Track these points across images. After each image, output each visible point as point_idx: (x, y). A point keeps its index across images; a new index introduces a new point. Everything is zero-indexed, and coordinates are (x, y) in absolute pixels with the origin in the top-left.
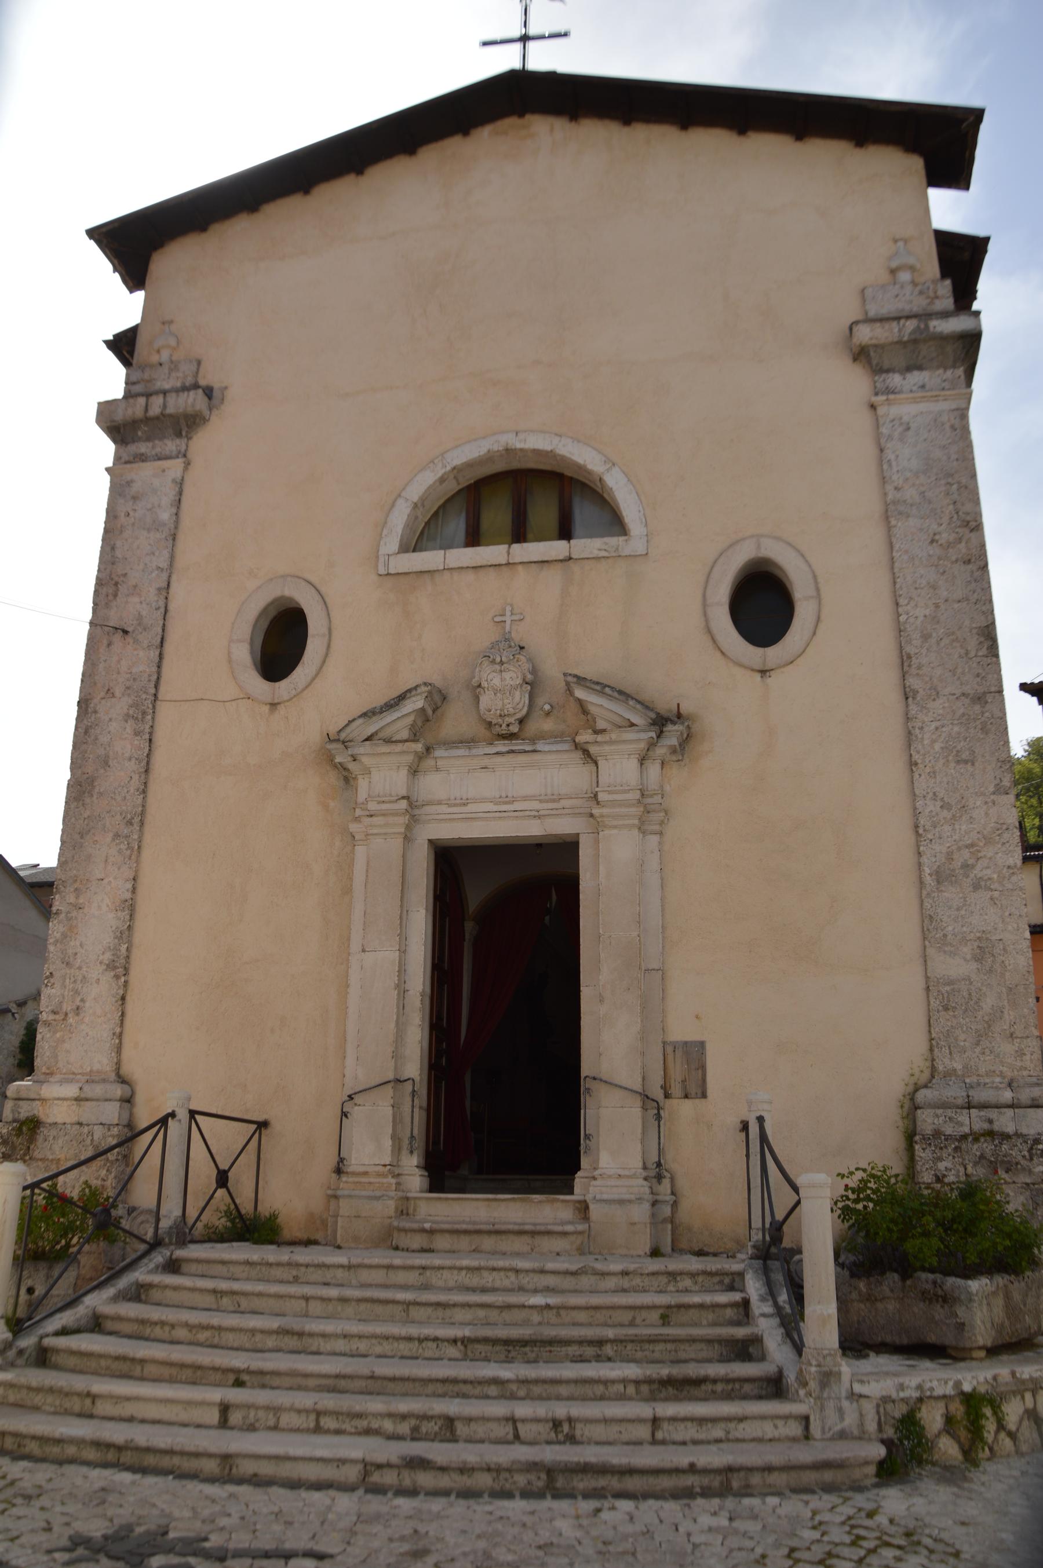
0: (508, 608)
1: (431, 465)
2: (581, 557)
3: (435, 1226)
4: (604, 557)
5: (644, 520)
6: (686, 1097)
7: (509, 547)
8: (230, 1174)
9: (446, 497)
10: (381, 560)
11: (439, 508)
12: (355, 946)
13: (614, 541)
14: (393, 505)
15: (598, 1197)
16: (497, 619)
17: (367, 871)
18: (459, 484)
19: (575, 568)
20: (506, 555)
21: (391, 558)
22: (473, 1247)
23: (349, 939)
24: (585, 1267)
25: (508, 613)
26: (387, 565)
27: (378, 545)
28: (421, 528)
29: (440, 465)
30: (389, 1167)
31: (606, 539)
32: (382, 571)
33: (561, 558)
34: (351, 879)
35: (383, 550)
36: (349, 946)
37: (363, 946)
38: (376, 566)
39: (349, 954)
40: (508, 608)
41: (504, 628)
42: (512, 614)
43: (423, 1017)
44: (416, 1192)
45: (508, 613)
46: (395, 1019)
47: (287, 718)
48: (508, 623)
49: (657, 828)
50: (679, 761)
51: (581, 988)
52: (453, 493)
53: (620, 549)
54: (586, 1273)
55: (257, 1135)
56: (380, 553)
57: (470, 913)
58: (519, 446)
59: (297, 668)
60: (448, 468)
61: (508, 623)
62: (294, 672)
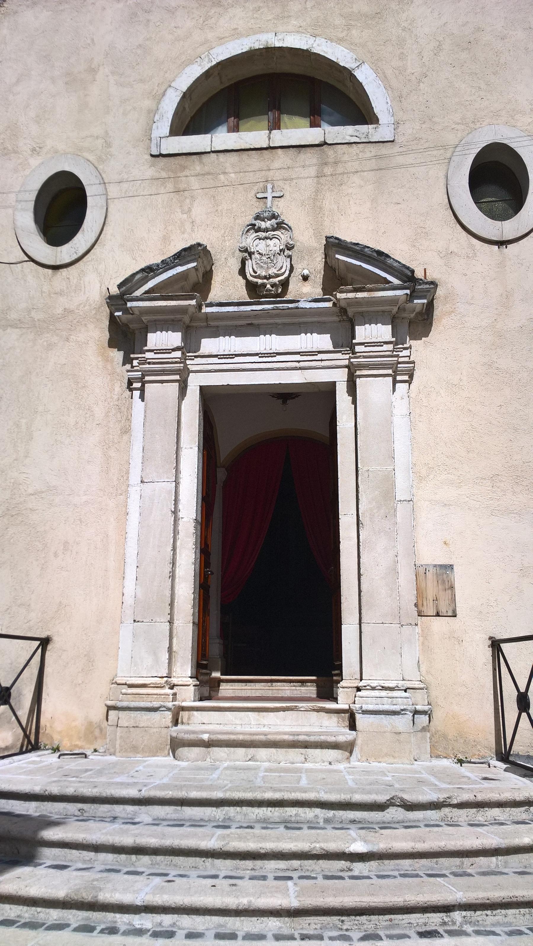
0: (269, 186)
1: (199, 60)
2: (335, 142)
3: (214, 737)
4: (355, 143)
5: (391, 111)
6: (438, 615)
7: (270, 133)
8: (12, 691)
9: (209, 95)
10: (154, 142)
11: (204, 104)
12: (135, 477)
13: (363, 128)
14: (164, 94)
15: (365, 707)
16: (259, 196)
17: (145, 412)
18: (221, 83)
19: (329, 151)
20: (267, 139)
21: (162, 140)
22: (250, 757)
23: (128, 473)
24: (392, 798)
25: (269, 190)
26: (159, 146)
27: (151, 129)
28: (187, 123)
29: (207, 59)
30: (165, 679)
31: (357, 127)
32: (155, 152)
33: (317, 143)
34: (129, 420)
35: (155, 134)
36: (128, 479)
37: (142, 477)
38: (149, 148)
39: (128, 486)
40: (269, 186)
41: (265, 203)
42: (273, 191)
43: (196, 541)
44: (191, 701)
45: (269, 190)
46: (172, 542)
47: (68, 278)
48: (270, 199)
49: (406, 378)
50: (424, 319)
51: (340, 517)
52: (215, 92)
53: (370, 137)
54: (394, 805)
55: (40, 650)
56: (152, 136)
57: (222, 459)
58: (278, 45)
59: (78, 235)
60: (214, 63)
61: (270, 199)
62: (75, 238)
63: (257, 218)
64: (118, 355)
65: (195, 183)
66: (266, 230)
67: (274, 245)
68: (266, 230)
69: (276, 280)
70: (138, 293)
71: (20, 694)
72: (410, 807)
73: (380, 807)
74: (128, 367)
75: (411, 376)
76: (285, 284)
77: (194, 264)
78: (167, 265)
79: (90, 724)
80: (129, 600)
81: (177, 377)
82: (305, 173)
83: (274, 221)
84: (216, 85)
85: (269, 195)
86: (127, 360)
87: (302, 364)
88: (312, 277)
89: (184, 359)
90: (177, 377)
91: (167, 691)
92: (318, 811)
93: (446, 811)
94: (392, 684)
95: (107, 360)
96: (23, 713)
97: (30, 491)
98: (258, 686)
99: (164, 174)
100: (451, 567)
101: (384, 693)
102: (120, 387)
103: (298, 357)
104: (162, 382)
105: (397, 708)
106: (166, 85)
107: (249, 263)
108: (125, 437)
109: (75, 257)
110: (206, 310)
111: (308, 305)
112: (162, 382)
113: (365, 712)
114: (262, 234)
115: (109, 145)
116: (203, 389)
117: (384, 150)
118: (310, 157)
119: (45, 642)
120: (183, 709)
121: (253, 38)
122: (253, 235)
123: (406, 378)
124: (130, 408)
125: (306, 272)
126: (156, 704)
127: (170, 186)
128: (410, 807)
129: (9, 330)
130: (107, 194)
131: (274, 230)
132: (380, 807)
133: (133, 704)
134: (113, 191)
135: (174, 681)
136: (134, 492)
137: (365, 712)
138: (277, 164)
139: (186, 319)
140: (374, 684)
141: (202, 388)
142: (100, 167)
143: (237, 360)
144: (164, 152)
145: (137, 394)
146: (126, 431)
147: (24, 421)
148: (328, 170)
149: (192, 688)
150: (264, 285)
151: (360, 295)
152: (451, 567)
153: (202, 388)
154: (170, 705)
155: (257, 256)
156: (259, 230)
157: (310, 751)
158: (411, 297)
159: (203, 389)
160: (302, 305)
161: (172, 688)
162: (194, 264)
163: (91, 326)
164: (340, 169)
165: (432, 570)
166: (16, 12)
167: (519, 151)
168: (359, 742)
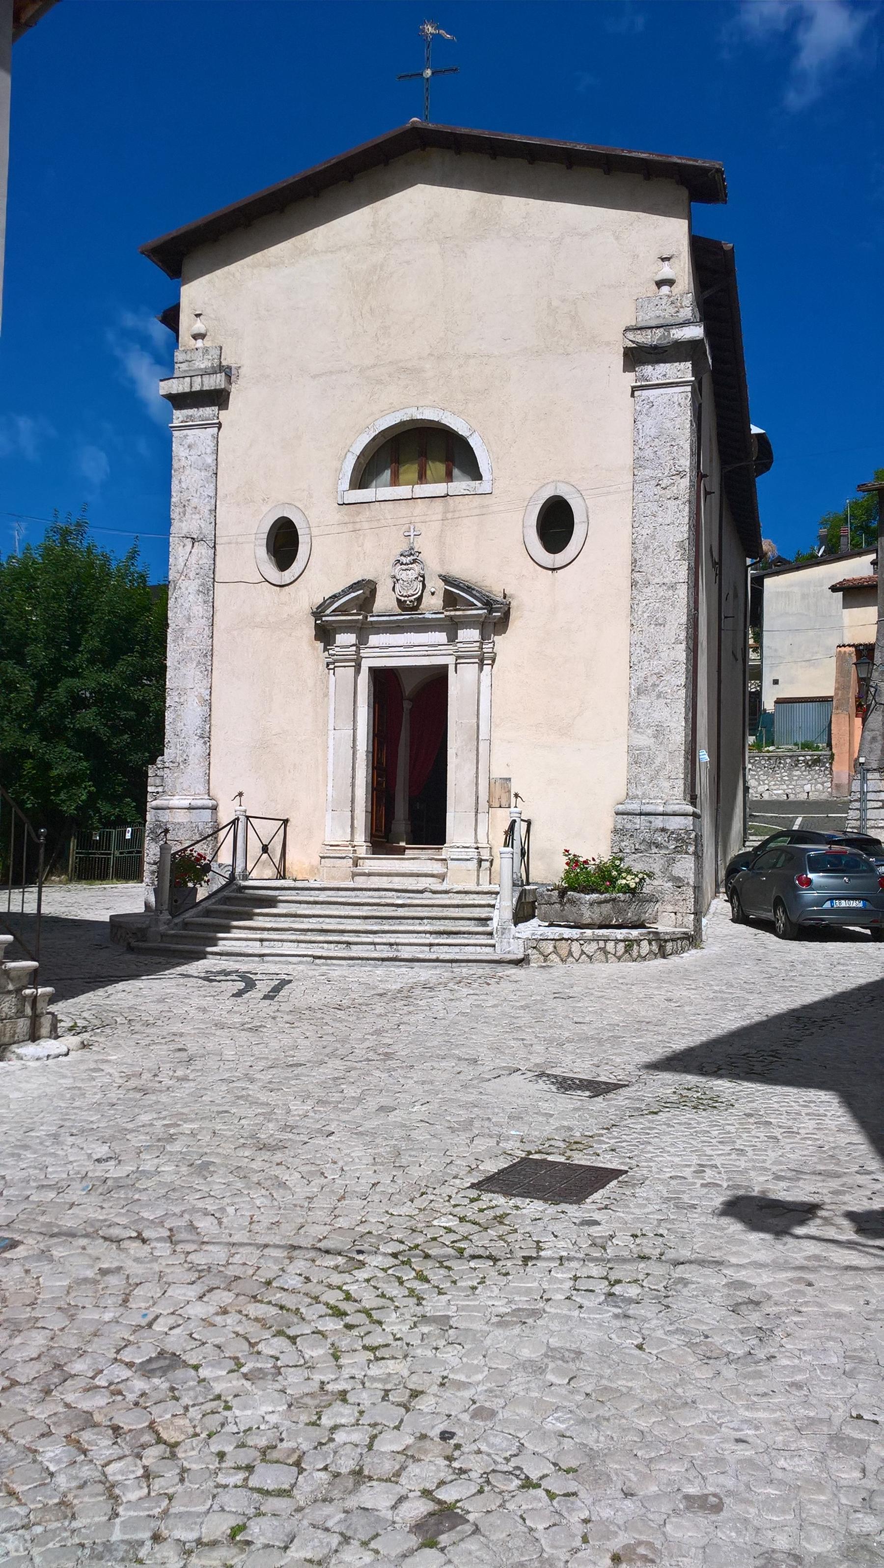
38: (336, 498)
49: (490, 662)
63: (402, 555)
64: (320, 645)
65: (366, 525)
66: (406, 564)
67: (412, 575)
68: (406, 564)
69: (412, 598)
70: (328, 612)
71: (274, 850)
72: (434, 892)
73: (421, 892)
74: (326, 653)
75: (494, 660)
76: (419, 599)
77: (361, 591)
78: (345, 592)
79: (312, 866)
80: (330, 798)
81: (353, 664)
82: (435, 517)
83: (412, 558)
84: (382, 441)
85: (412, 534)
86: (325, 649)
87: (429, 653)
88: (437, 593)
89: (358, 652)
90: (353, 664)
91: (350, 848)
92: (394, 893)
93: (451, 894)
94: (467, 845)
95: (315, 649)
96: (277, 860)
97: (273, 733)
98: (430, 851)
99: (346, 519)
100: (509, 779)
101: (463, 850)
102: (322, 666)
103: (426, 648)
104: (345, 667)
105: (468, 857)
106: (346, 450)
107: (397, 585)
108: (326, 699)
109: (293, 579)
110: (370, 619)
111: (431, 616)
112: (345, 667)
113: (452, 859)
114: (404, 567)
115: (311, 496)
116: (371, 669)
117: (486, 500)
118: (438, 504)
119: (285, 822)
120: (360, 858)
121: (402, 412)
122: (399, 567)
123: (490, 662)
124: (328, 681)
125: (433, 590)
126: (344, 855)
127: (350, 527)
128: (434, 892)
129: (256, 629)
130: (310, 534)
131: (412, 564)
132: (421, 892)
133: (331, 855)
134: (315, 531)
135: (355, 843)
136: (331, 733)
137: (452, 859)
138: (417, 511)
139: (359, 625)
140: (458, 845)
141: (370, 668)
142: (306, 513)
143: (390, 649)
144: (346, 502)
145: (332, 671)
146: (326, 695)
147: (267, 689)
148: (449, 516)
149: (365, 848)
150: (405, 601)
151: (458, 613)
152: (509, 779)
153: (370, 668)
154: (351, 855)
155: (401, 581)
156: (402, 564)
157: (420, 878)
158: (490, 611)
159: (371, 669)
160: (427, 616)
161: (354, 847)
162: (361, 591)
163: (304, 626)
164: (457, 515)
165: (499, 781)
166: (246, 388)
167: (570, 501)
168: (448, 874)
